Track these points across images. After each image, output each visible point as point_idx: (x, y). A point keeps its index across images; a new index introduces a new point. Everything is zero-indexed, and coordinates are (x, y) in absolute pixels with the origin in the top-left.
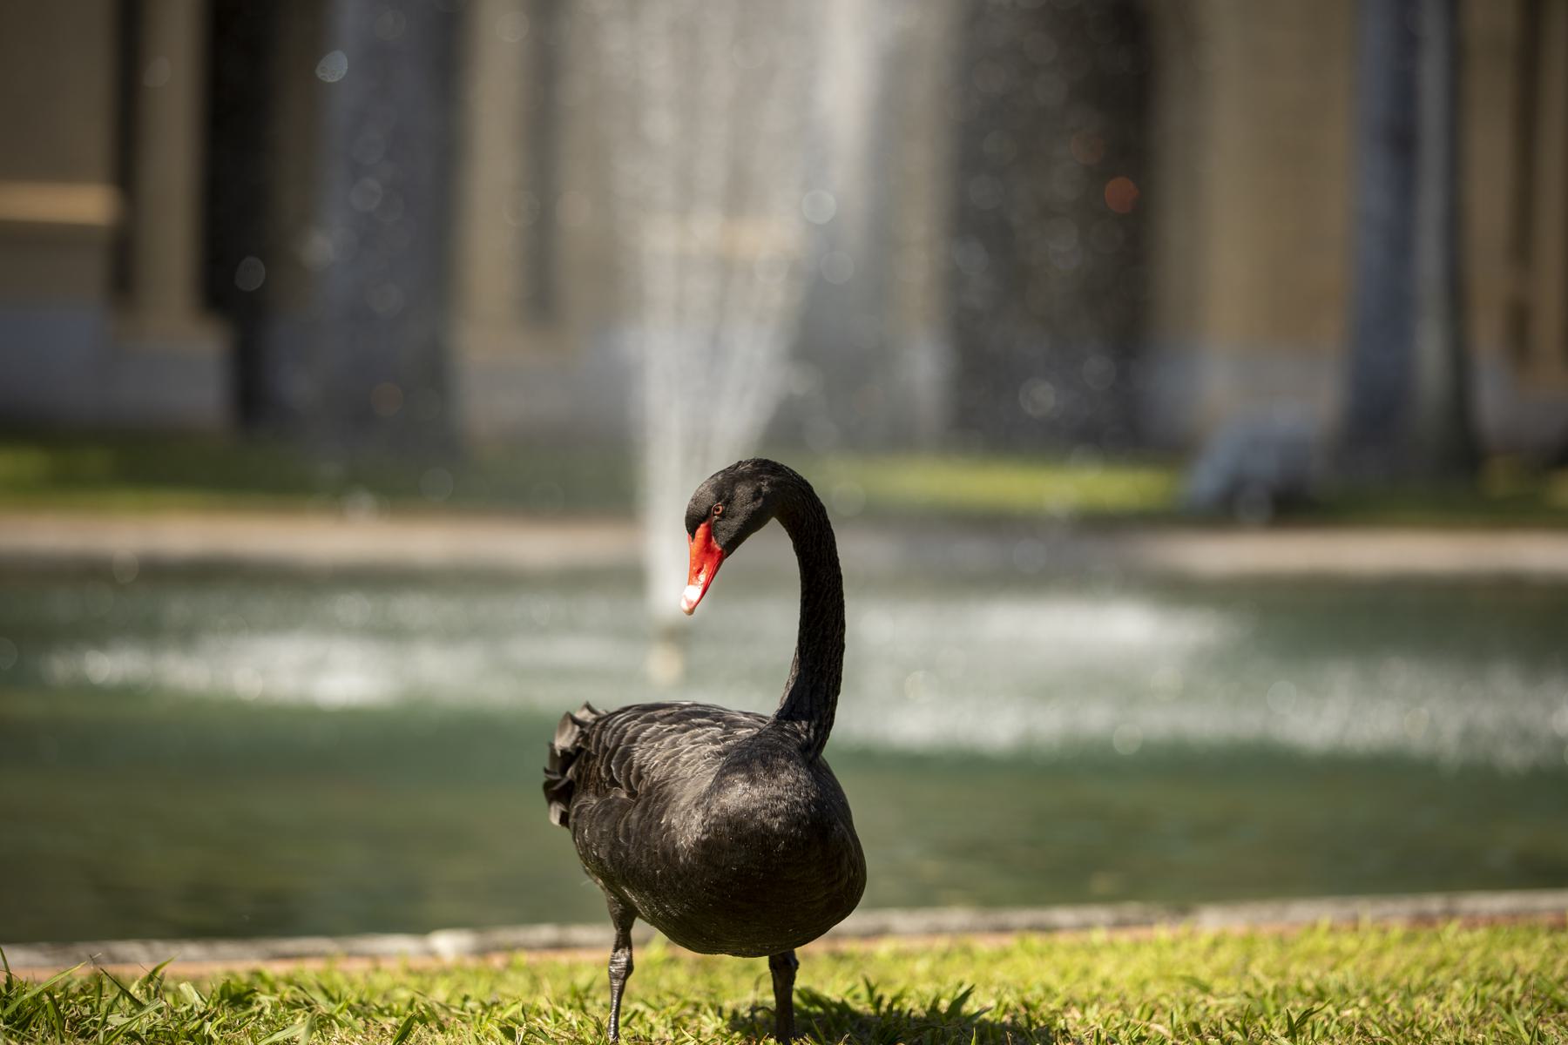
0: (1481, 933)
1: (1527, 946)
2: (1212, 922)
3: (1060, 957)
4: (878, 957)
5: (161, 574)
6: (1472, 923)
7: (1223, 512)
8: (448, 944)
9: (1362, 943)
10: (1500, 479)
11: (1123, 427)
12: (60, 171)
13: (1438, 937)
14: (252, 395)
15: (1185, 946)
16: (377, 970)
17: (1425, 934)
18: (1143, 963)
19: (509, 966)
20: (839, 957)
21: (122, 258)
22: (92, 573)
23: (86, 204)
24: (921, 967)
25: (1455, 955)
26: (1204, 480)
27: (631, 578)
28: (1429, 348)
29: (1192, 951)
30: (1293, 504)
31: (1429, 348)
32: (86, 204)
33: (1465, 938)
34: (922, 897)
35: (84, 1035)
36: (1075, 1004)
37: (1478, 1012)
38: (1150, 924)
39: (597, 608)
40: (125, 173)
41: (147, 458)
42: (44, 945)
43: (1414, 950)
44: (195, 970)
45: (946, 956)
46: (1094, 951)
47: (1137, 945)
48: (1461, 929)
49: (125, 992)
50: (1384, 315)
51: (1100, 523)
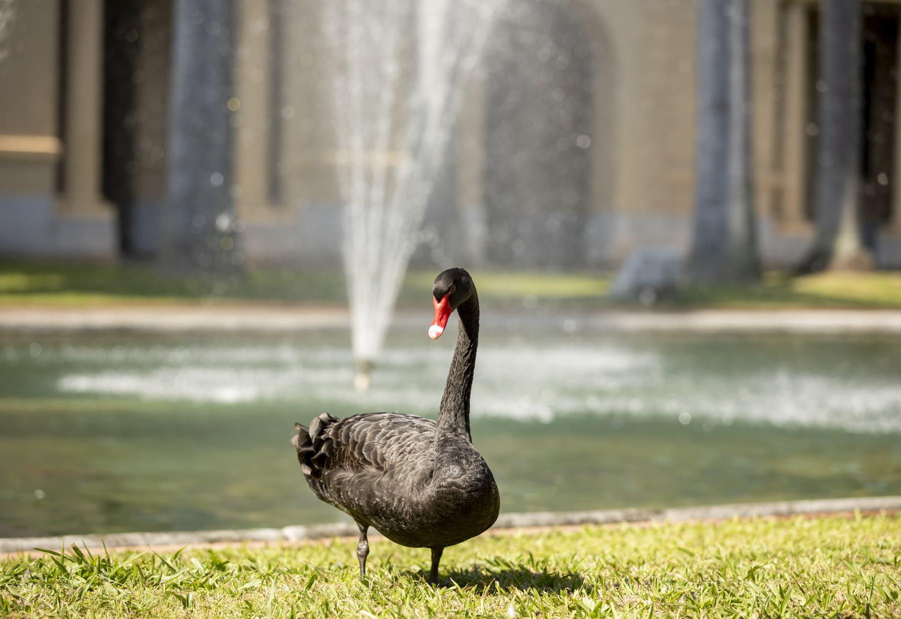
0: (815, 522)
1: (838, 529)
2: (674, 517)
3: (607, 537)
4: (515, 538)
5: (88, 336)
6: (808, 516)
7: (630, 301)
8: (293, 533)
9: (756, 528)
10: (772, 279)
11: (573, 256)
12: (31, 130)
13: (793, 524)
14: (126, 244)
15: (668, 531)
16: (267, 547)
17: (787, 523)
18: (649, 541)
19: (333, 544)
20: (497, 539)
21: (61, 173)
22: (52, 337)
23: (44, 145)
24: (539, 543)
25: (805, 534)
26: (622, 281)
27: (341, 337)
28: (736, 215)
29: (672, 533)
30: (670, 296)
31: (736, 215)
32: (44, 145)
33: (807, 525)
34: (520, 508)
35: (895, 595)
36: (633, 563)
37: (833, 565)
38: (647, 520)
39: (327, 355)
40: (62, 131)
41: (74, 275)
42: (92, 535)
43: (782, 533)
44: (190, 549)
45: (549, 537)
46: (623, 535)
47: (644, 530)
48: (803, 521)
49: (164, 563)
50: (713, 198)
51: (567, 304)
